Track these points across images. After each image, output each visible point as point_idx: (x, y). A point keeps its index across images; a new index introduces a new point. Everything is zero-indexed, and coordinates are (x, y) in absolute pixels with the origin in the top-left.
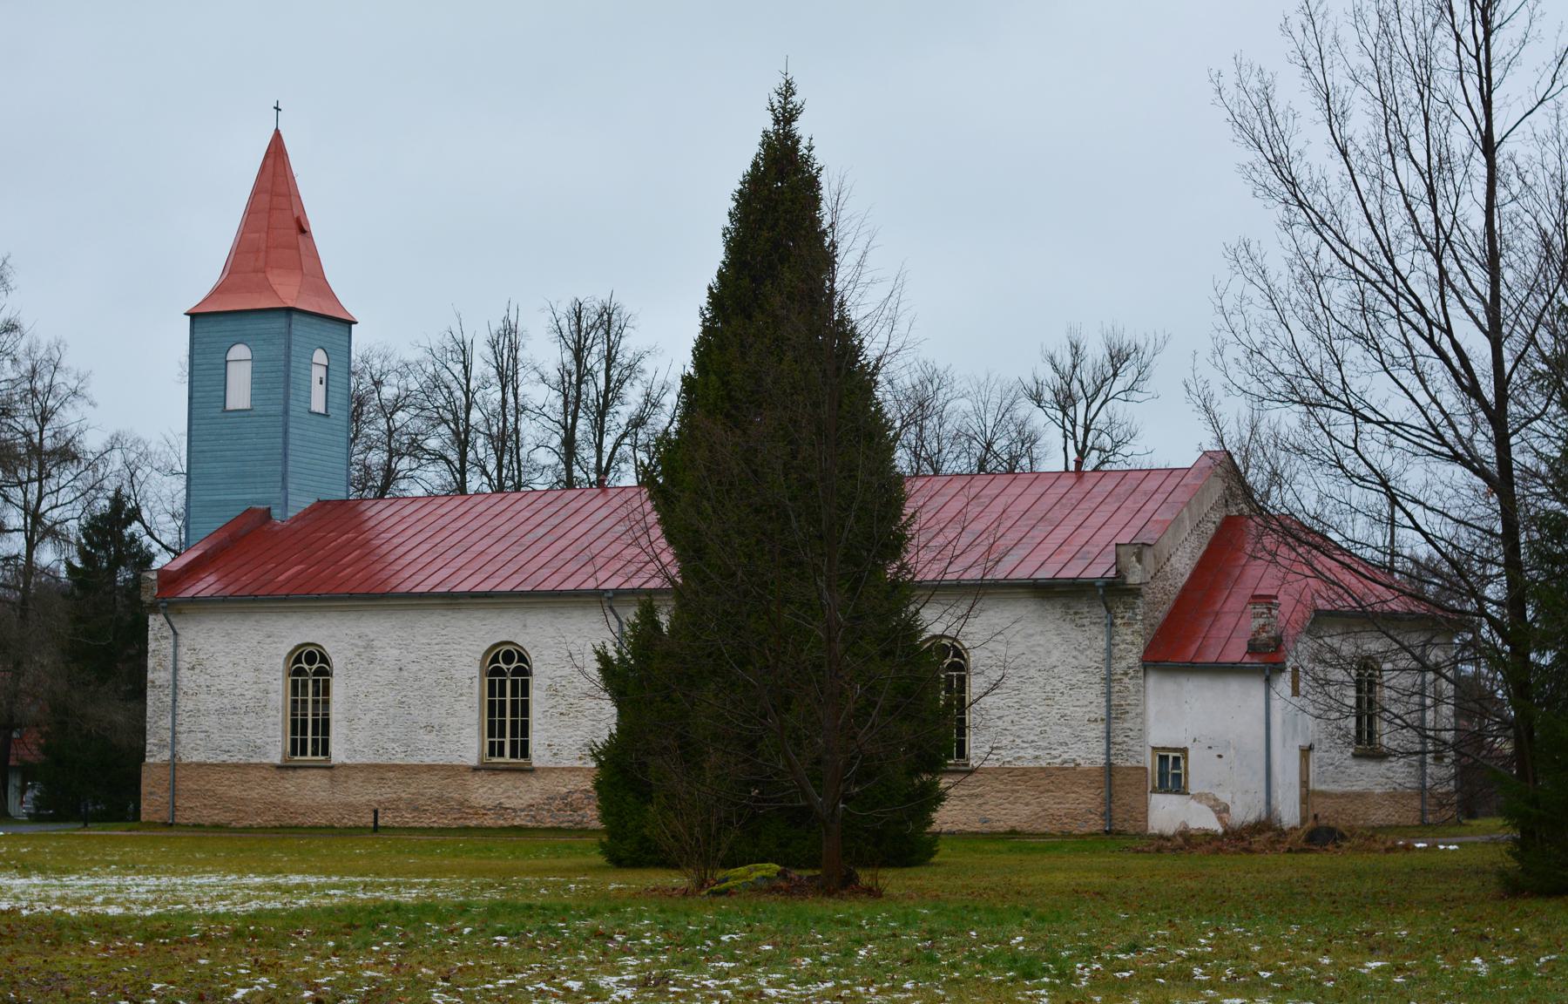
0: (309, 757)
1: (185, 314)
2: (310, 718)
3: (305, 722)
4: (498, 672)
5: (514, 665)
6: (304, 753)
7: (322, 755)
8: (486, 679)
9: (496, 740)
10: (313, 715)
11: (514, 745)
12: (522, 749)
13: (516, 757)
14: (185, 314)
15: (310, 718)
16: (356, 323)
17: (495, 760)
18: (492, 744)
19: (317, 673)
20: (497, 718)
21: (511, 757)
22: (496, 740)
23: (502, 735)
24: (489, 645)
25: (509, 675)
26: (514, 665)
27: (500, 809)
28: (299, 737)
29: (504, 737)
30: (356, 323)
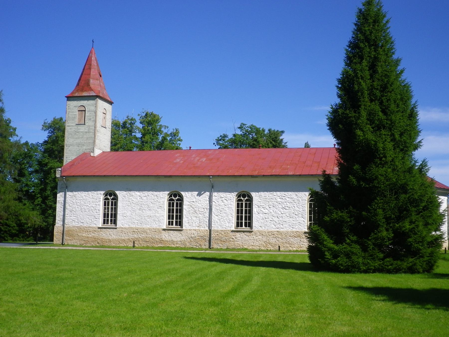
0: (109, 224)
1: (66, 97)
2: (110, 213)
3: (108, 214)
4: (172, 200)
5: (177, 198)
6: (242, 226)
7: (114, 224)
8: (168, 202)
9: (171, 220)
10: (111, 212)
11: (176, 222)
12: (249, 225)
13: (177, 226)
14: (66, 97)
15: (110, 213)
16: (113, 103)
17: (170, 226)
18: (169, 222)
19: (178, 200)
20: (240, 215)
21: (111, 224)
22: (171, 220)
23: (173, 219)
24: (242, 191)
25: (175, 201)
26: (177, 198)
27: (173, 242)
28: (240, 221)
29: (173, 219)
30: (113, 103)
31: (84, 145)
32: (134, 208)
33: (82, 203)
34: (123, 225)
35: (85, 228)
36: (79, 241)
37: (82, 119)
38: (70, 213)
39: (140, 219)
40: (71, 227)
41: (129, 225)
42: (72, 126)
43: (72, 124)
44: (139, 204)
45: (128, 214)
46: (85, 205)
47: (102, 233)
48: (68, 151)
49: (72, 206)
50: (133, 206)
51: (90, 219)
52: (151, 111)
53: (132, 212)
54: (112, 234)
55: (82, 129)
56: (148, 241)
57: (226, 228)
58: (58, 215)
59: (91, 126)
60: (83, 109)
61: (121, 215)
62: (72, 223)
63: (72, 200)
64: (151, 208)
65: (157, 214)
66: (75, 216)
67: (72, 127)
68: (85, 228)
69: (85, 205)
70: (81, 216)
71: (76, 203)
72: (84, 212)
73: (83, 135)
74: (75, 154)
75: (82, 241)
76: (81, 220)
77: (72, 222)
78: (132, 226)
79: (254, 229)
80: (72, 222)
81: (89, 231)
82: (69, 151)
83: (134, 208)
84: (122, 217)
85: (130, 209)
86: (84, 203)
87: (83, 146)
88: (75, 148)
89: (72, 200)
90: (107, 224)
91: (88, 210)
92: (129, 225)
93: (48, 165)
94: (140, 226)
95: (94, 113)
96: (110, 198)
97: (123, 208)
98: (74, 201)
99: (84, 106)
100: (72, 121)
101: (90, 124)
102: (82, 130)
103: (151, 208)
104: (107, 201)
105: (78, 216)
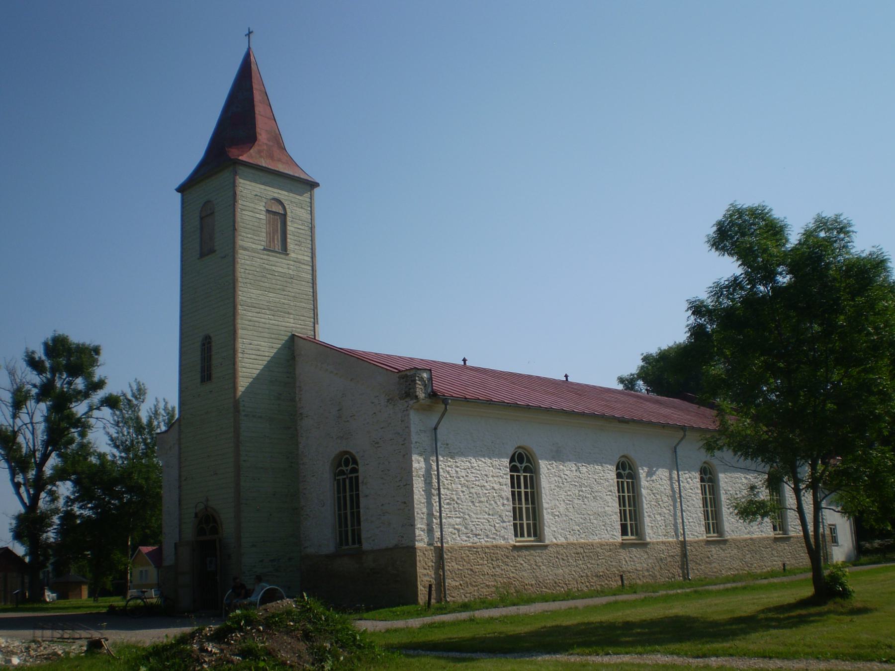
13: (522, 535)
17: (518, 539)
31: (289, 313)
32: (569, 493)
33: (471, 477)
34: (555, 538)
35: (487, 550)
36: (476, 588)
37: (276, 237)
38: (448, 506)
39: (583, 521)
40: (456, 547)
41: (566, 538)
42: (254, 251)
43: (254, 246)
44: (576, 484)
45: (562, 510)
46: (477, 483)
47: (523, 562)
48: (247, 322)
49: (450, 487)
50: (567, 488)
51: (492, 523)
52: (732, 274)
53: (567, 504)
54: (541, 564)
55: (281, 265)
56: (602, 576)
57: (697, 537)
58: (420, 512)
59: (302, 261)
60: (278, 209)
61: (549, 510)
62: (454, 536)
63: (448, 469)
64: (596, 494)
65: (607, 508)
66: (458, 515)
67: (254, 254)
68: (487, 550)
69: (477, 483)
70: (474, 516)
71: (459, 478)
72: (477, 505)
73: (285, 284)
74: (266, 335)
75: (482, 588)
76: (473, 528)
77: (455, 534)
78: (572, 539)
79: (549, 536)
80: (455, 534)
81: (494, 559)
82: (250, 323)
83: (569, 493)
84: (551, 517)
85: (563, 496)
86: (474, 479)
87: (287, 315)
88: (267, 316)
89: (448, 469)
90: (521, 537)
91: (485, 499)
92: (566, 538)
93: (889, 366)
94: (584, 539)
95: (306, 228)
96: (521, 467)
97: (551, 492)
98: (453, 472)
99: (283, 201)
100: (255, 237)
101: (300, 257)
102: (280, 270)
103: (596, 494)
104: (515, 474)
105: (467, 517)
